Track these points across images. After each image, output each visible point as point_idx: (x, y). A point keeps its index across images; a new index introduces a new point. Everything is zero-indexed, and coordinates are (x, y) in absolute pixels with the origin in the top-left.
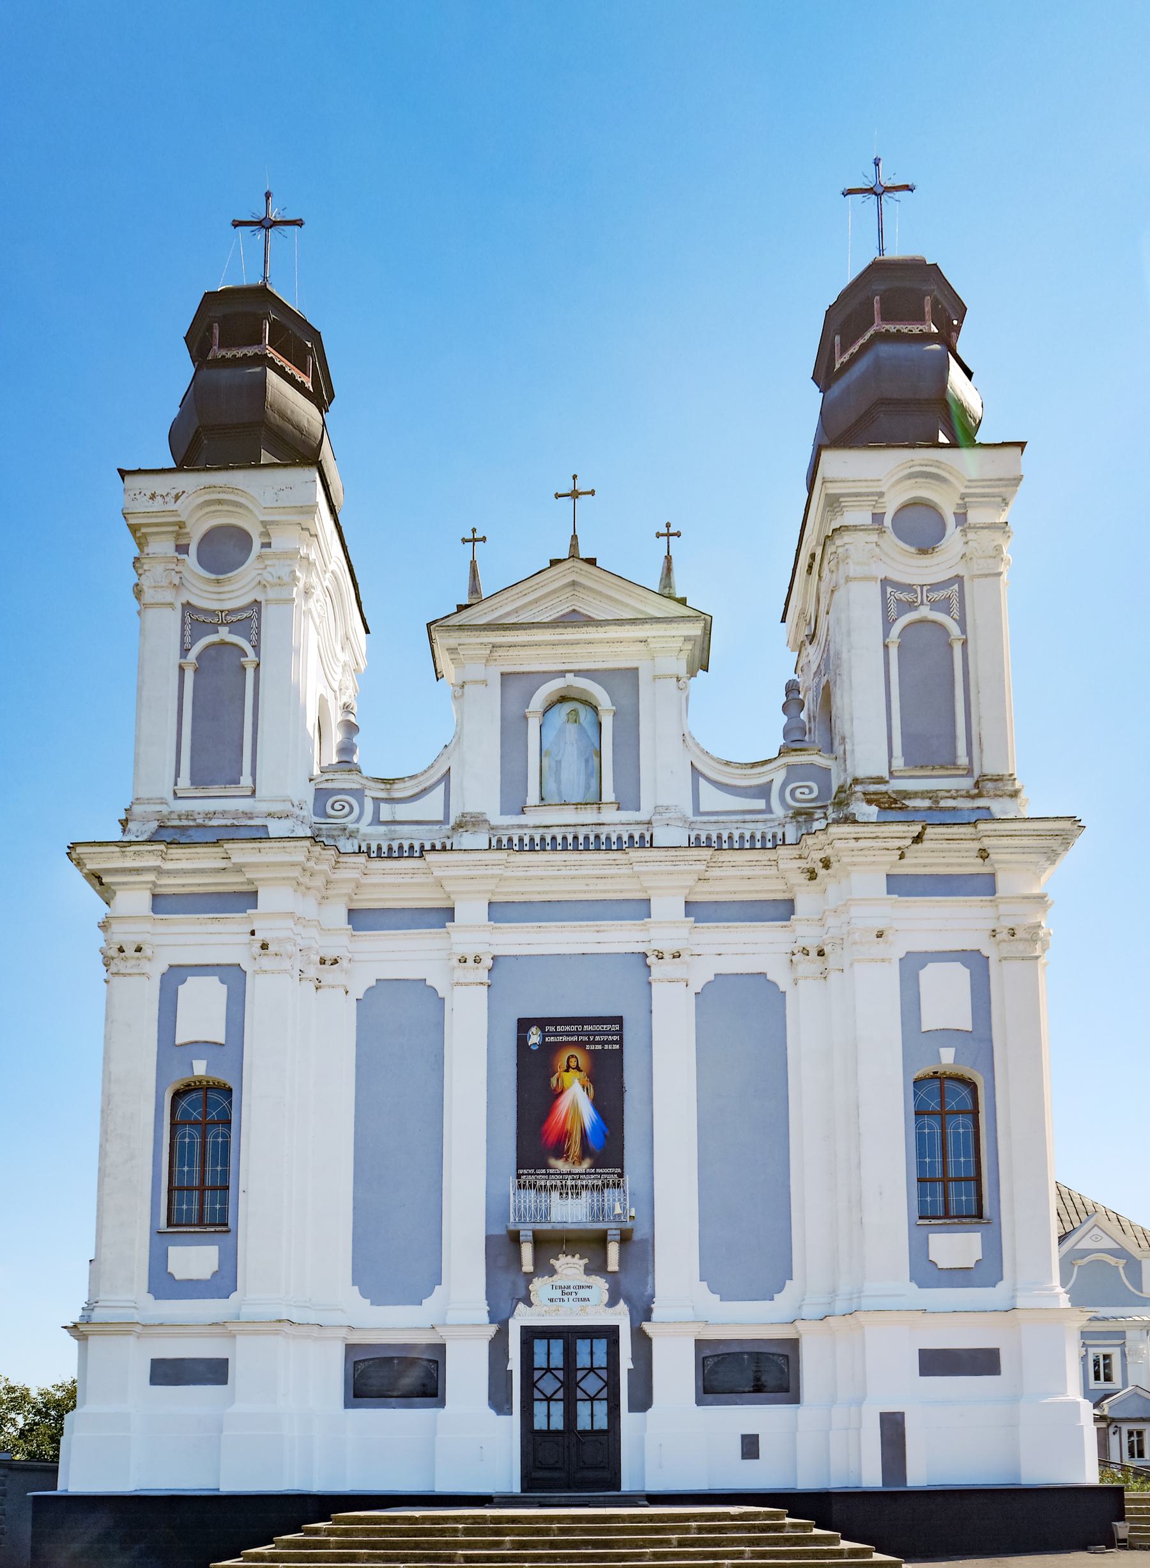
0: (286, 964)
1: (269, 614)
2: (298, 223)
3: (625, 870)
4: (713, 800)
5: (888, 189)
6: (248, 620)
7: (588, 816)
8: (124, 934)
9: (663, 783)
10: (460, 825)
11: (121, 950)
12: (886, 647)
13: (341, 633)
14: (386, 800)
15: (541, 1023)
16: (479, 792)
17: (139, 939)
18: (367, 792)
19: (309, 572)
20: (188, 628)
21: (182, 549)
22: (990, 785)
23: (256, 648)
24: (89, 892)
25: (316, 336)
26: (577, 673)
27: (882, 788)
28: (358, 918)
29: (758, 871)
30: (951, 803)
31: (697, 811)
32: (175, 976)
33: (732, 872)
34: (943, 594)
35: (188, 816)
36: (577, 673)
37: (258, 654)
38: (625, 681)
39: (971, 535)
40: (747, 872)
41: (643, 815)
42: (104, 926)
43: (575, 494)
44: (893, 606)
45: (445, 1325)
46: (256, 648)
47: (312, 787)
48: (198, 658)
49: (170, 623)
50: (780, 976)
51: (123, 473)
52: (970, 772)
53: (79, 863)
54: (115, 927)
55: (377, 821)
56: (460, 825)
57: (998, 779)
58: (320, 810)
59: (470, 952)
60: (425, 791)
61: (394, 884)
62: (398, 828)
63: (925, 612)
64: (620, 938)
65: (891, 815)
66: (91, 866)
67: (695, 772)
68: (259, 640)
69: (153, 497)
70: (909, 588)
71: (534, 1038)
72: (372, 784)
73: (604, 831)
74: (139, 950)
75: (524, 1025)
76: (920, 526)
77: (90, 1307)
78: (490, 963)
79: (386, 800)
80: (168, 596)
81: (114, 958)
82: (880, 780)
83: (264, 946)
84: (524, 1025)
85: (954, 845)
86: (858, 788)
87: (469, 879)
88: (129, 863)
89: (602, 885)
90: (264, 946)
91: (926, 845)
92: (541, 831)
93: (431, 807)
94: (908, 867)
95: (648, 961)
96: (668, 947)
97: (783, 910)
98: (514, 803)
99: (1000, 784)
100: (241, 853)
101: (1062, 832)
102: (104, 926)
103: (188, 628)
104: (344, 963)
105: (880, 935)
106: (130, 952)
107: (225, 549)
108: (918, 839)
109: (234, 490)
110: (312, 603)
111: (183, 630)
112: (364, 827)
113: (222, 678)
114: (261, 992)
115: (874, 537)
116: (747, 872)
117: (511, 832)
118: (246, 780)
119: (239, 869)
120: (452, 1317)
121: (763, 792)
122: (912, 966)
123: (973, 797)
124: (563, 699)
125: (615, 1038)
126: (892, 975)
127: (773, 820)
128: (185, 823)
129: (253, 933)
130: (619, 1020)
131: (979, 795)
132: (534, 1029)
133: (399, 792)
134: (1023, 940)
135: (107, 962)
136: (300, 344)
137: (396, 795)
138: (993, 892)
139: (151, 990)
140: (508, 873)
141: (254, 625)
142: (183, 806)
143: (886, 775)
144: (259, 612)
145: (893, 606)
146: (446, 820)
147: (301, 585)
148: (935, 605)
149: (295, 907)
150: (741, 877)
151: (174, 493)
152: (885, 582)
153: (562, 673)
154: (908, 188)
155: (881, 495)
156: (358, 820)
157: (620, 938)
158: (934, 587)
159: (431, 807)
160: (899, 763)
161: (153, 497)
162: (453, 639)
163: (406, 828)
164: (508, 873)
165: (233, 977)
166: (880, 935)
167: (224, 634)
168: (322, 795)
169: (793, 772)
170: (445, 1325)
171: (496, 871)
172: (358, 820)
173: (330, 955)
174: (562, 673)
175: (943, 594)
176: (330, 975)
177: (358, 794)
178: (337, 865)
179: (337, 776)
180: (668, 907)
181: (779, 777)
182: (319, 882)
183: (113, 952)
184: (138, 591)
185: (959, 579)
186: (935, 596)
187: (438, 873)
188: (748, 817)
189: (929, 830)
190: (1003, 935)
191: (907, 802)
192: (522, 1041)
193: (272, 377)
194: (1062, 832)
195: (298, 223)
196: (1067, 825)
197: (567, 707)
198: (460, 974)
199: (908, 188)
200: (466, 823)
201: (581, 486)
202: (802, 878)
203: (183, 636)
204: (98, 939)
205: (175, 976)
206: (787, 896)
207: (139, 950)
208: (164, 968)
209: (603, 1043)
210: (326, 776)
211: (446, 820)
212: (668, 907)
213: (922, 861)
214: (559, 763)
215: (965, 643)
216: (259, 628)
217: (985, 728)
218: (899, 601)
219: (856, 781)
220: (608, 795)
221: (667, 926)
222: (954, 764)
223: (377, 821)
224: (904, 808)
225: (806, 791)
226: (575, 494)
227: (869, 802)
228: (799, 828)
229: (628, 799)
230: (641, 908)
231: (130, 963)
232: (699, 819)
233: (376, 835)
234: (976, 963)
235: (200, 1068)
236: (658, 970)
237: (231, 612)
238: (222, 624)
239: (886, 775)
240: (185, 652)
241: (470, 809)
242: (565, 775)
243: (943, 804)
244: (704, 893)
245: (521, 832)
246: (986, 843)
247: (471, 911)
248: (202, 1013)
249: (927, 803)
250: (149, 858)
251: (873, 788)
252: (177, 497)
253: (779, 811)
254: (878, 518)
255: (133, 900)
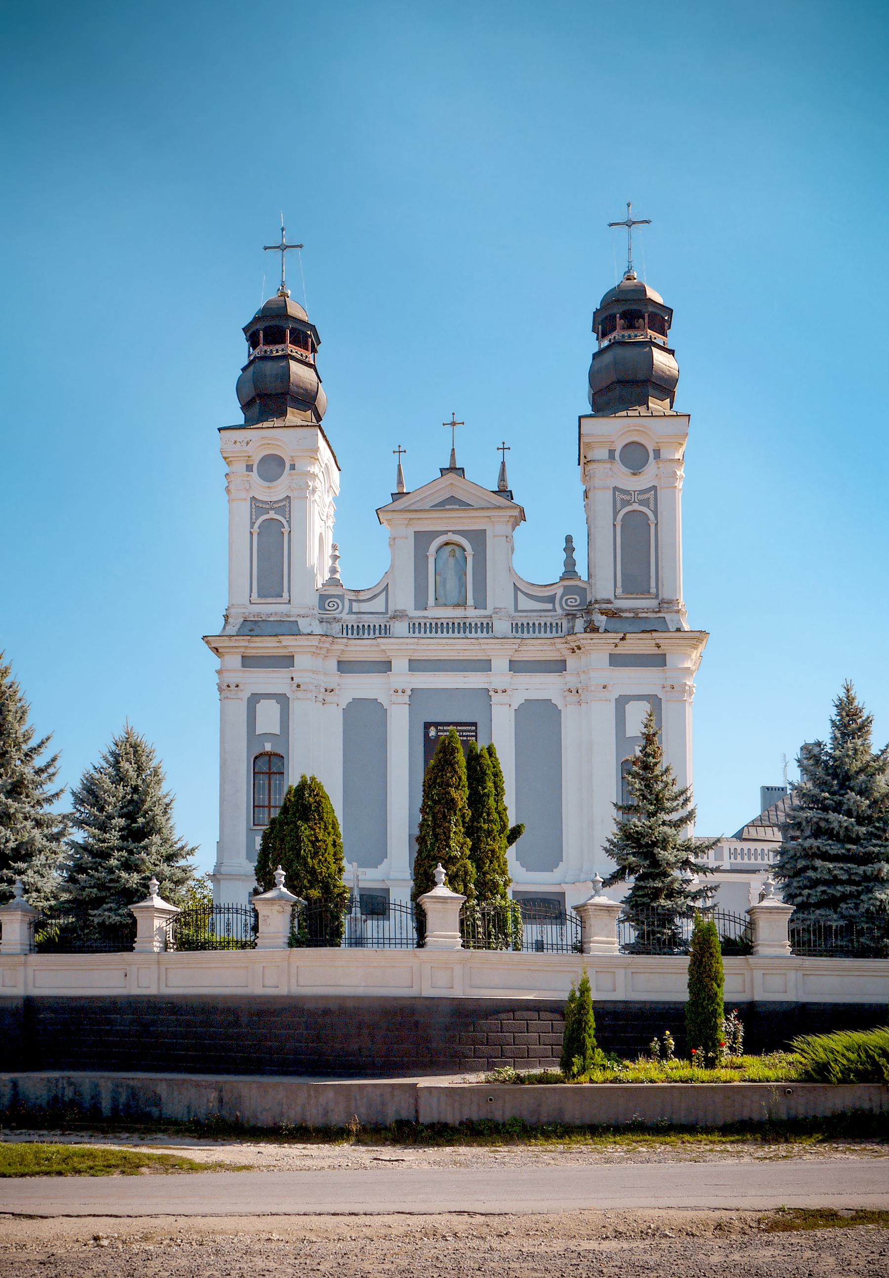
0: (310, 695)
1: (295, 504)
2: (301, 246)
3: (477, 647)
4: (525, 603)
5: (634, 223)
6: (284, 506)
7: (459, 613)
8: (231, 678)
9: (499, 595)
10: (394, 617)
11: (228, 686)
12: (614, 525)
13: (327, 486)
14: (355, 601)
15: (436, 725)
16: (403, 598)
17: (237, 681)
18: (346, 596)
19: (314, 481)
20: (254, 510)
21: (249, 468)
22: (665, 605)
23: (289, 522)
24: (212, 655)
25: (313, 328)
26: (454, 532)
27: (609, 606)
28: (344, 667)
29: (545, 648)
30: (644, 615)
31: (516, 610)
32: (254, 700)
33: (532, 648)
34: (646, 496)
35: (259, 615)
36: (454, 532)
37: (290, 527)
38: (478, 538)
39: (661, 465)
40: (540, 648)
41: (488, 612)
42: (219, 672)
43: (453, 424)
44: (618, 502)
45: (389, 879)
46: (289, 522)
47: (318, 594)
48: (259, 528)
49: (245, 509)
50: (557, 701)
51: (219, 430)
52: (657, 596)
53: (207, 642)
54: (226, 674)
55: (351, 612)
56: (394, 617)
57: (670, 602)
58: (322, 607)
59: (400, 688)
60: (375, 596)
61: (362, 649)
62: (362, 616)
63: (636, 507)
64: (474, 681)
65: (613, 620)
66: (213, 645)
67: (516, 588)
68: (290, 518)
69: (235, 442)
70: (627, 492)
71: (432, 732)
72: (349, 593)
73: (468, 621)
74: (237, 686)
75: (427, 726)
76: (635, 456)
77: (219, 865)
78: (409, 693)
79: (355, 601)
80: (243, 495)
81: (224, 688)
82: (609, 602)
83: (298, 686)
84: (427, 726)
85: (641, 641)
86: (597, 606)
87: (400, 648)
88: (232, 644)
89: (467, 653)
90: (298, 686)
91: (628, 641)
92: (435, 621)
93: (378, 605)
94: (620, 650)
95: (490, 693)
96: (500, 688)
97: (560, 666)
98: (421, 603)
99: (671, 605)
100: (287, 641)
101: (699, 637)
102: (219, 672)
103: (254, 510)
104: (336, 691)
105: (604, 687)
106: (233, 687)
107: (272, 466)
108: (623, 639)
109: (276, 439)
110: (316, 497)
111: (251, 512)
112: (345, 616)
113: (272, 539)
114: (297, 708)
115: (609, 466)
116: (540, 648)
117: (420, 621)
118: (285, 595)
119: (285, 647)
120: (393, 875)
121: (551, 599)
122: (622, 702)
123: (657, 612)
124: (447, 544)
125: (474, 734)
126: (610, 709)
127: (556, 616)
128: (256, 619)
129: (292, 679)
130: (475, 724)
131: (659, 612)
132: (432, 728)
133: (362, 596)
134: (678, 690)
135: (220, 690)
136: (304, 336)
137: (361, 598)
138: (664, 664)
139: (243, 706)
140: (419, 647)
141: (287, 509)
142: (256, 609)
143: (612, 598)
144: (290, 503)
145: (618, 502)
146: (386, 613)
147: (311, 488)
148: (641, 502)
149: (312, 665)
150: (537, 649)
151: (246, 441)
152: (615, 489)
153: (446, 532)
154: (647, 222)
155: (613, 442)
156: (341, 613)
157: (474, 681)
158: (642, 492)
159: (378, 605)
160: (619, 591)
161: (235, 442)
162: (389, 516)
163: (366, 616)
164: (419, 647)
165: (283, 700)
166: (604, 687)
167: (272, 515)
168: (323, 598)
169: (567, 590)
170: (389, 879)
171: (412, 647)
172: (341, 613)
173: (330, 688)
174: (446, 532)
175: (646, 496)
176: (330, 697)
177: (341, 597)
178: (332, 643)
179: (330, 588)
180: (500, 664)
181: (559, 592)
182: (324, 652)
183: (224, 687)
184: (228, 490)
185: (654, 488)
186: (641, 497)
187: (383, 647)
188: (543, 614)
189: (628, 635)
190: (668, 689)
191: (621, 614)
192: (426, 734)
193: (294, 366)
194: (699, 637)
195: (301, 246)
196: (698, 634)
197: (450, 548)
198: (394, 698)
199: (647, 222)
200: (398, 616)
201: (458, 419)
202: (569, 652)
203: (251, 515)
204: (216, 679)
205: (254, 700)
206: (562, 658)
207: (237, 686)
208: (249, 695)
209: (467, 736)
210: (325, 588)
211: (386, 613)
212: (500, 664)
213: (626, 648)
214: (445, 579)
215: (657, 524)
216: (290, 511)
217: (664, 574)
218: (622, 499)
219: (596, 602)
220: (470, 601)
221: (499, 676)
222: (649, 592)
223: (351, 612)
224: (620, 617)
225: (573, 601)
226: (453, 424)
227: (602, 614)
228: (569, 622)
229: (480, 604)
230: (485, 666)
231: (232, 693)
232: (517, 614)
233: (351, 620)
234: (283, 700)
235: (268, 747)
236: (495, 698)
237: (276, 502)
238: (272, 509)
239: (612, 598)
240: (252, 524)
241: (399, 607)
242: (448, 586)
243: (640, 615)
244: (518, 657)
245: (425, 621)
246: (658, 641)
247: (400, 664)
248: (268, 718)
249: (632, 615)
250: (242, 642)
251: (604, 606)
252: (248, 443)
253: (559, 611)
254: (612, 453)
255: (234, 661)
